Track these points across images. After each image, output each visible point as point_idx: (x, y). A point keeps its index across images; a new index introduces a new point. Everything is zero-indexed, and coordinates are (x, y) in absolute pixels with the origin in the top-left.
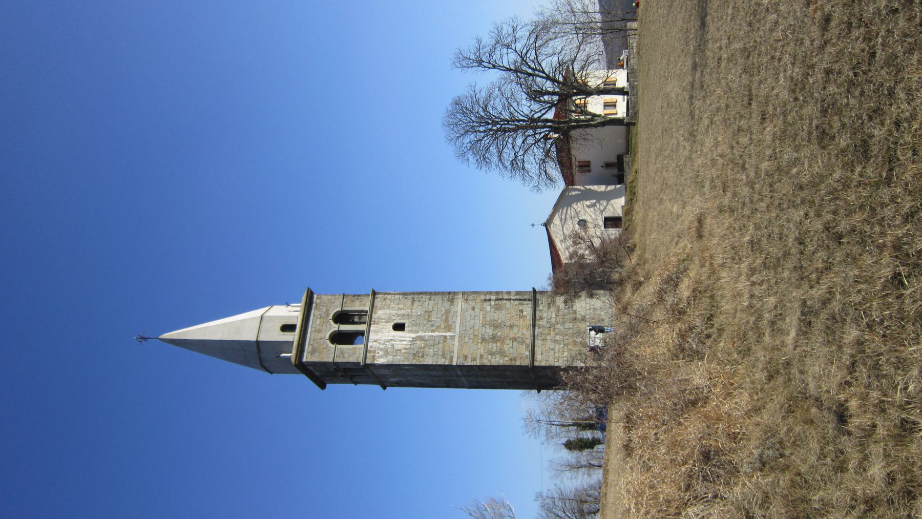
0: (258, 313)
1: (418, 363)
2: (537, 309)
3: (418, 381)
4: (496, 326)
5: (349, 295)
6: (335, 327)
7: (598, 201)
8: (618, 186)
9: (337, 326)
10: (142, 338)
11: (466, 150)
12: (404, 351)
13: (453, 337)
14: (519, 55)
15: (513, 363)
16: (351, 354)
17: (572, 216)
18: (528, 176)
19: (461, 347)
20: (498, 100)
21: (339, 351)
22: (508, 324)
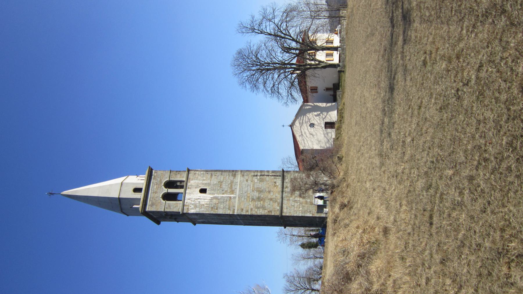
0: (119, 180)
1: (214, 213)
2: (284, 182)
3: (214, 221)
4: (260, 191)
5: (173, 171)
6: (165, 190)
7: (322, 113)
8: (333, 104)
9: (166, 189)
10: (50, 194)
11: (244, 81)
12: (206, 205)
13: (235, 198)
14: (276, 26)
15: (270, 214)
16: (174, 206)
17: (307, 121)
18: (280, 96)
19: (240, 203)
20: (264, 51)
21: (167, 205)
22: (267, 190)
